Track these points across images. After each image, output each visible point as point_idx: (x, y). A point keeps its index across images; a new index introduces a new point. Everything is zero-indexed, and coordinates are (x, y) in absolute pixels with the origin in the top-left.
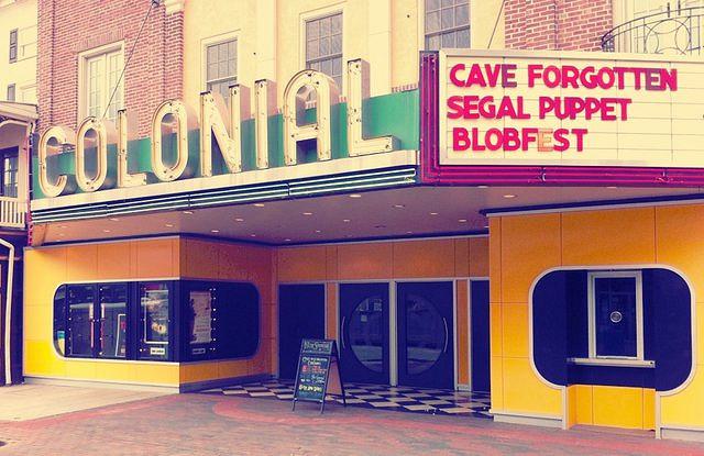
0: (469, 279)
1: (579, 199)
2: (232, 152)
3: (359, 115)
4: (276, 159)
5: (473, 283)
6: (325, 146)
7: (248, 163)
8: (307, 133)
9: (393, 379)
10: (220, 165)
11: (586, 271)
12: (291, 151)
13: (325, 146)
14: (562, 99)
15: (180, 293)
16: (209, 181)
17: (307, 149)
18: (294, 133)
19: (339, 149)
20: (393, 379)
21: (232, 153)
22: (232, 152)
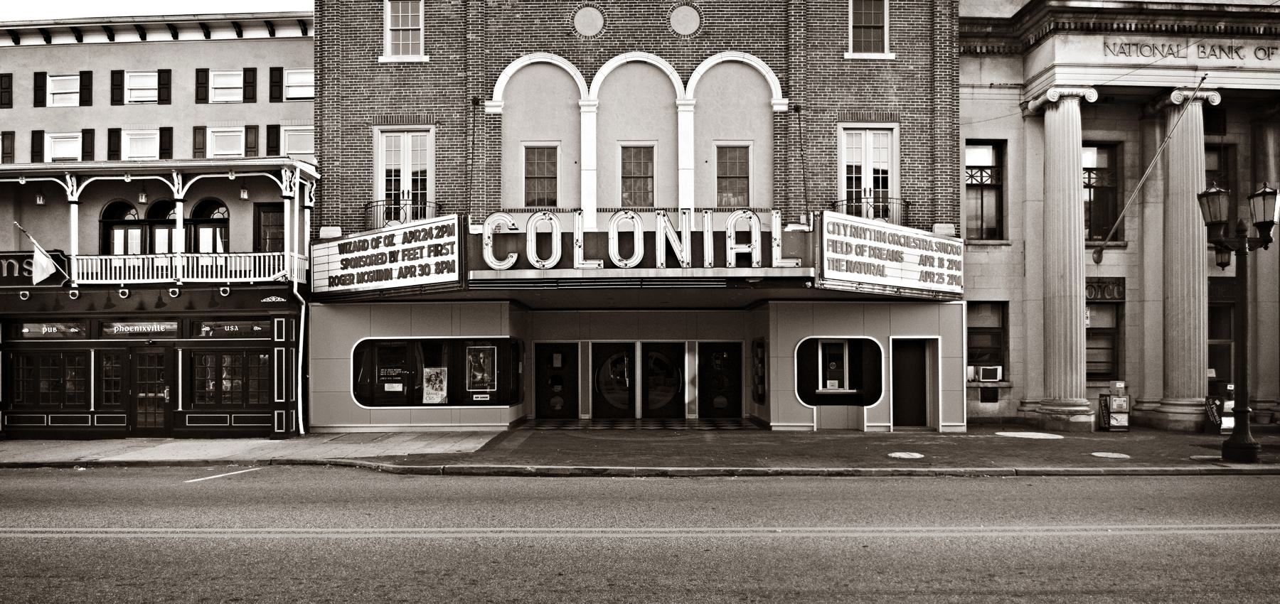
0: (697, 342)
1: (800, 296)
2: (684, 252)
3: (774, 244)
4: (720, 260)
5: (593, 344)
6: (757, 257)
7: (697, 260)
8: (744, 249)
9: (639, 413)
10: (672, 260)
11: (969, 329)
12: (731, 258)
13: (757, 257)
14: (578, 236)
15: (509, 350)
16: (661, 271)
17: (744, 260)
18: (733, 249)
19: (767, 261)
20: (639, 413)
21: (684, 254)
22: (684, 252)
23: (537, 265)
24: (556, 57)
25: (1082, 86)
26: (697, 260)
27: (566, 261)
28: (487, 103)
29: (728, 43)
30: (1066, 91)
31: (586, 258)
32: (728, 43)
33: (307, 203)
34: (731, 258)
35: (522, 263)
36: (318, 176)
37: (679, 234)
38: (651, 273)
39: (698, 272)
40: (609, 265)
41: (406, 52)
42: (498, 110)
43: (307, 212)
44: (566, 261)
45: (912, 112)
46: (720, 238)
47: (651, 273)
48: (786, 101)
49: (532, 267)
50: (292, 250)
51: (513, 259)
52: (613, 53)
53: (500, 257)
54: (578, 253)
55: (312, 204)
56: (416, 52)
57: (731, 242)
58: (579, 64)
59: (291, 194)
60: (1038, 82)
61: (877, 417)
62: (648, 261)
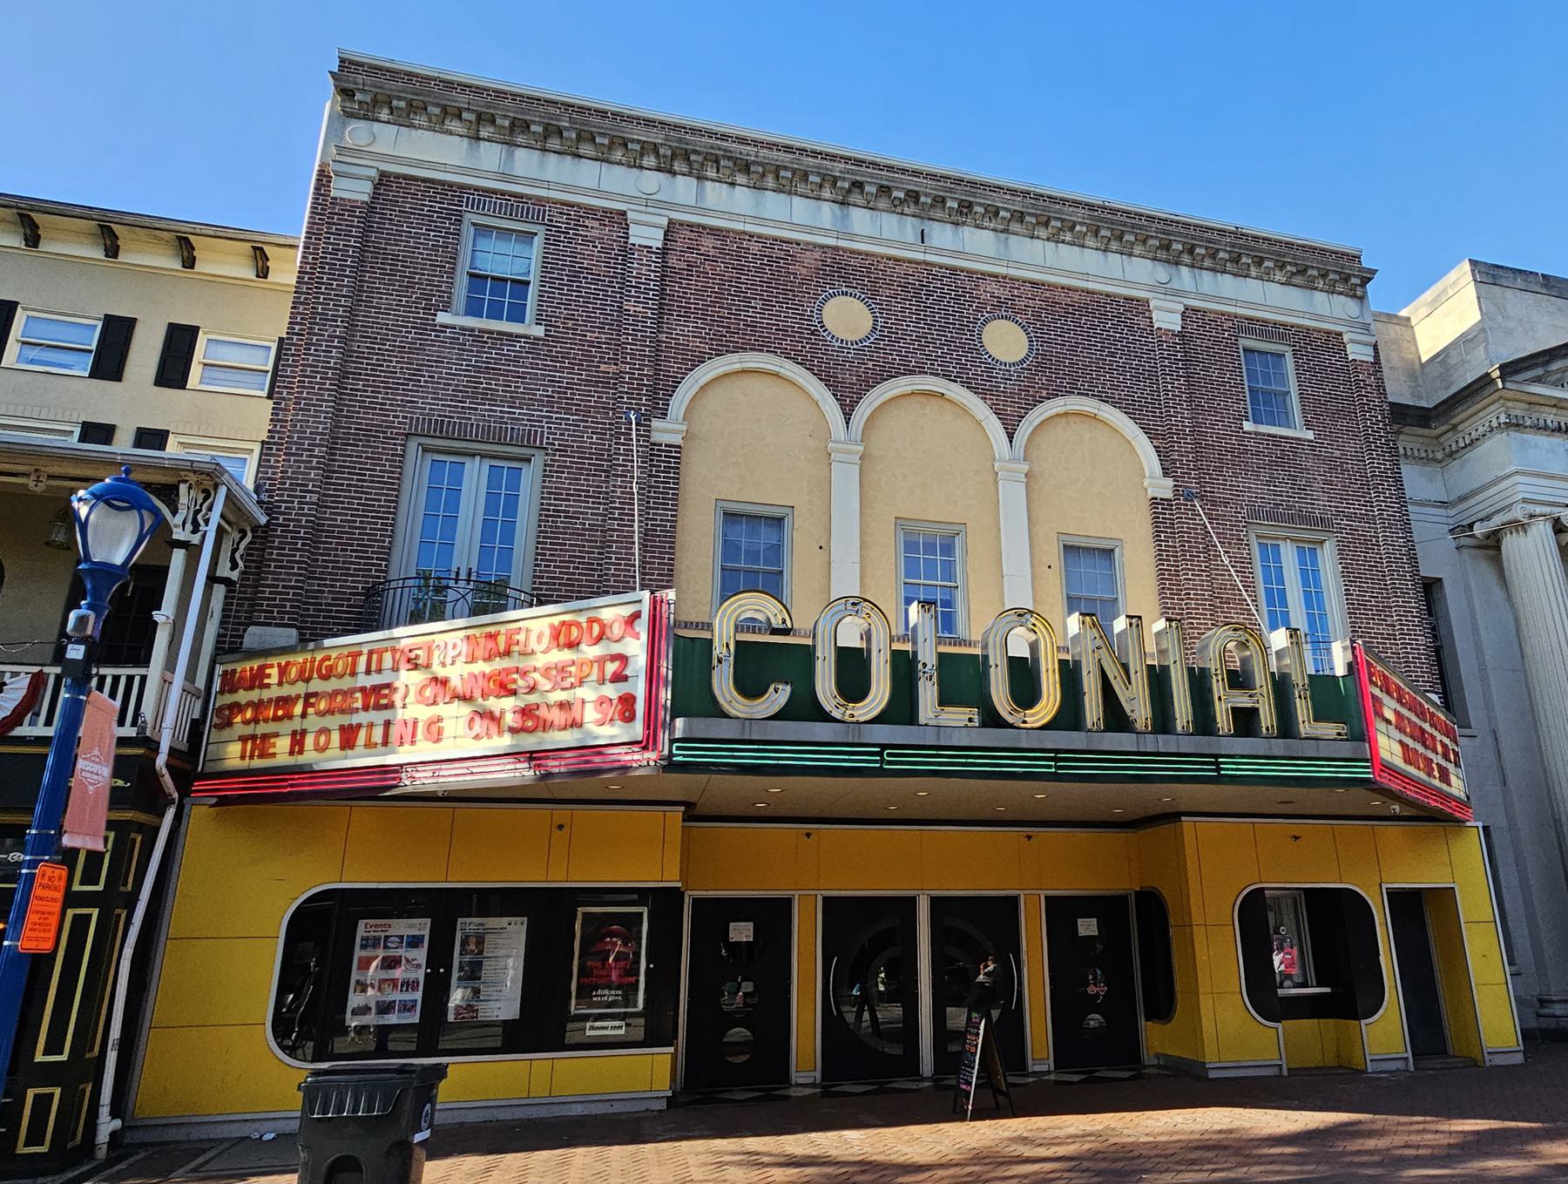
2: (1139, 707)
6: (1267, 718)
7: (1163, 721)
10: (1116, 718)
12: (1223, 721)
13: (1267, 718)
16: (1092, 733)
17: (1245, 721)
18: (1224, 702)
22: (1139, 707)
23: (836, 714)
24: (789, 364)
25: (1553, 504)
26: (1163, 721)
27: (902, 708)
28: (655, 423)
29: (1073, 384)
30: (1539, 510)
31: (944, 701)
32: (1073, 384)
33: (224, 570)
34: (1223, 721)
35: (805, 707)
36: (263, 520)
37: (1126, 667)
38: (1074, 740)
39: (1164, 743)
40: (992, 719)
41: (495, 314)
42: (676, 439)
43: (220, 591)
44: (902, 708)
45: (1349, 518)
46: (1199, 682)
47: (1074, 740)
48: (1170, 482)
49: (826, 717)
50: (170, 665)
51: (778, 696)
52: (886, 374)
53: (750, 687)
54: (928, 692)
55: (235, 575)
56: (517, 315)
57: (1218, 688)
58: (829, 380)
59: (196, 539)
60: (1479, 498)
61: (1385, 1032)
62: (1069, 717)
